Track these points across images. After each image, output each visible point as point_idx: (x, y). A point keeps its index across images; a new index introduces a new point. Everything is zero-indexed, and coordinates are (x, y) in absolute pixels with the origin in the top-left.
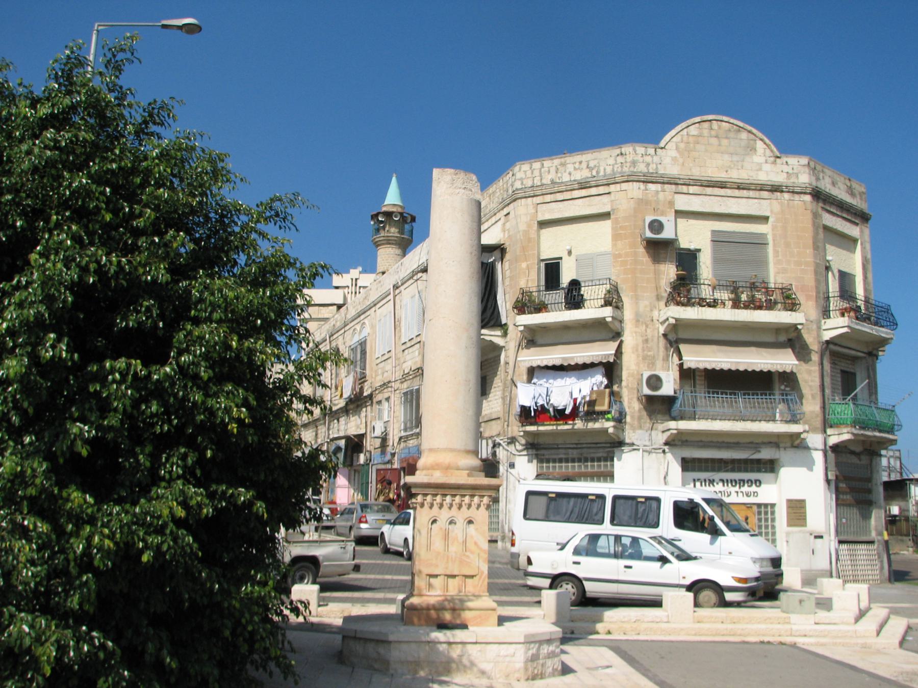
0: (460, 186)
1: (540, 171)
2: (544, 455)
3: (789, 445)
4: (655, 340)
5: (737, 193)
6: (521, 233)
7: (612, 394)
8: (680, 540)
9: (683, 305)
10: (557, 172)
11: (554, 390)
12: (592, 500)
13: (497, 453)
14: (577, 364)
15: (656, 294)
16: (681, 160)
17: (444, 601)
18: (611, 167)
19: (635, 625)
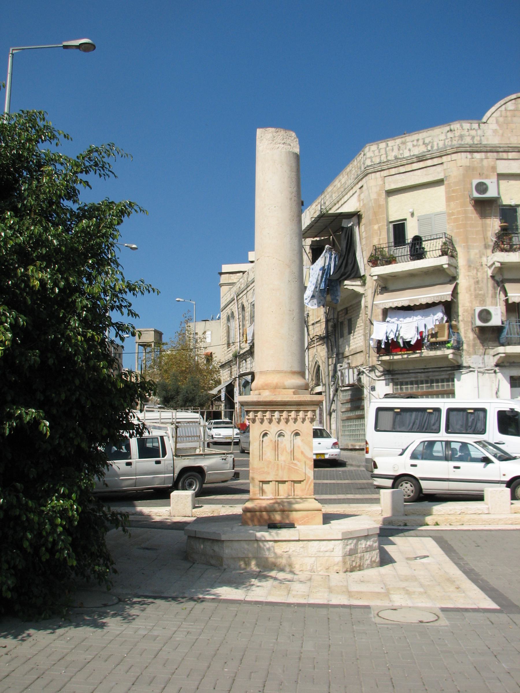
0: (279, 141)
2: (398, 379)
4: (485, 281)
6: (373, 201)
7: (451, 327)
8: (504, 443)
9: (506, 251)
10: (399, 150)
11: (403, 325)
12: (430, 413)
13: (362, 379)
14: (421, 304)
15: (483, 243)
16: (501, 132)
17: (274, 503)
18: (443, 142)
19: (459, 517)
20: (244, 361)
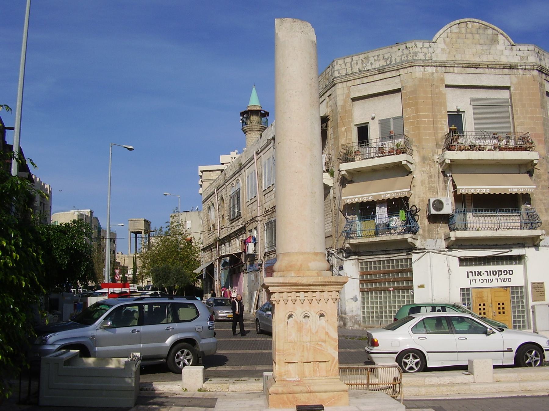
1: (351, 64)
3: (531, 245)
4: (437, 175)
5: (487, 71)
18: (400, 57)
20: (223, 245)
